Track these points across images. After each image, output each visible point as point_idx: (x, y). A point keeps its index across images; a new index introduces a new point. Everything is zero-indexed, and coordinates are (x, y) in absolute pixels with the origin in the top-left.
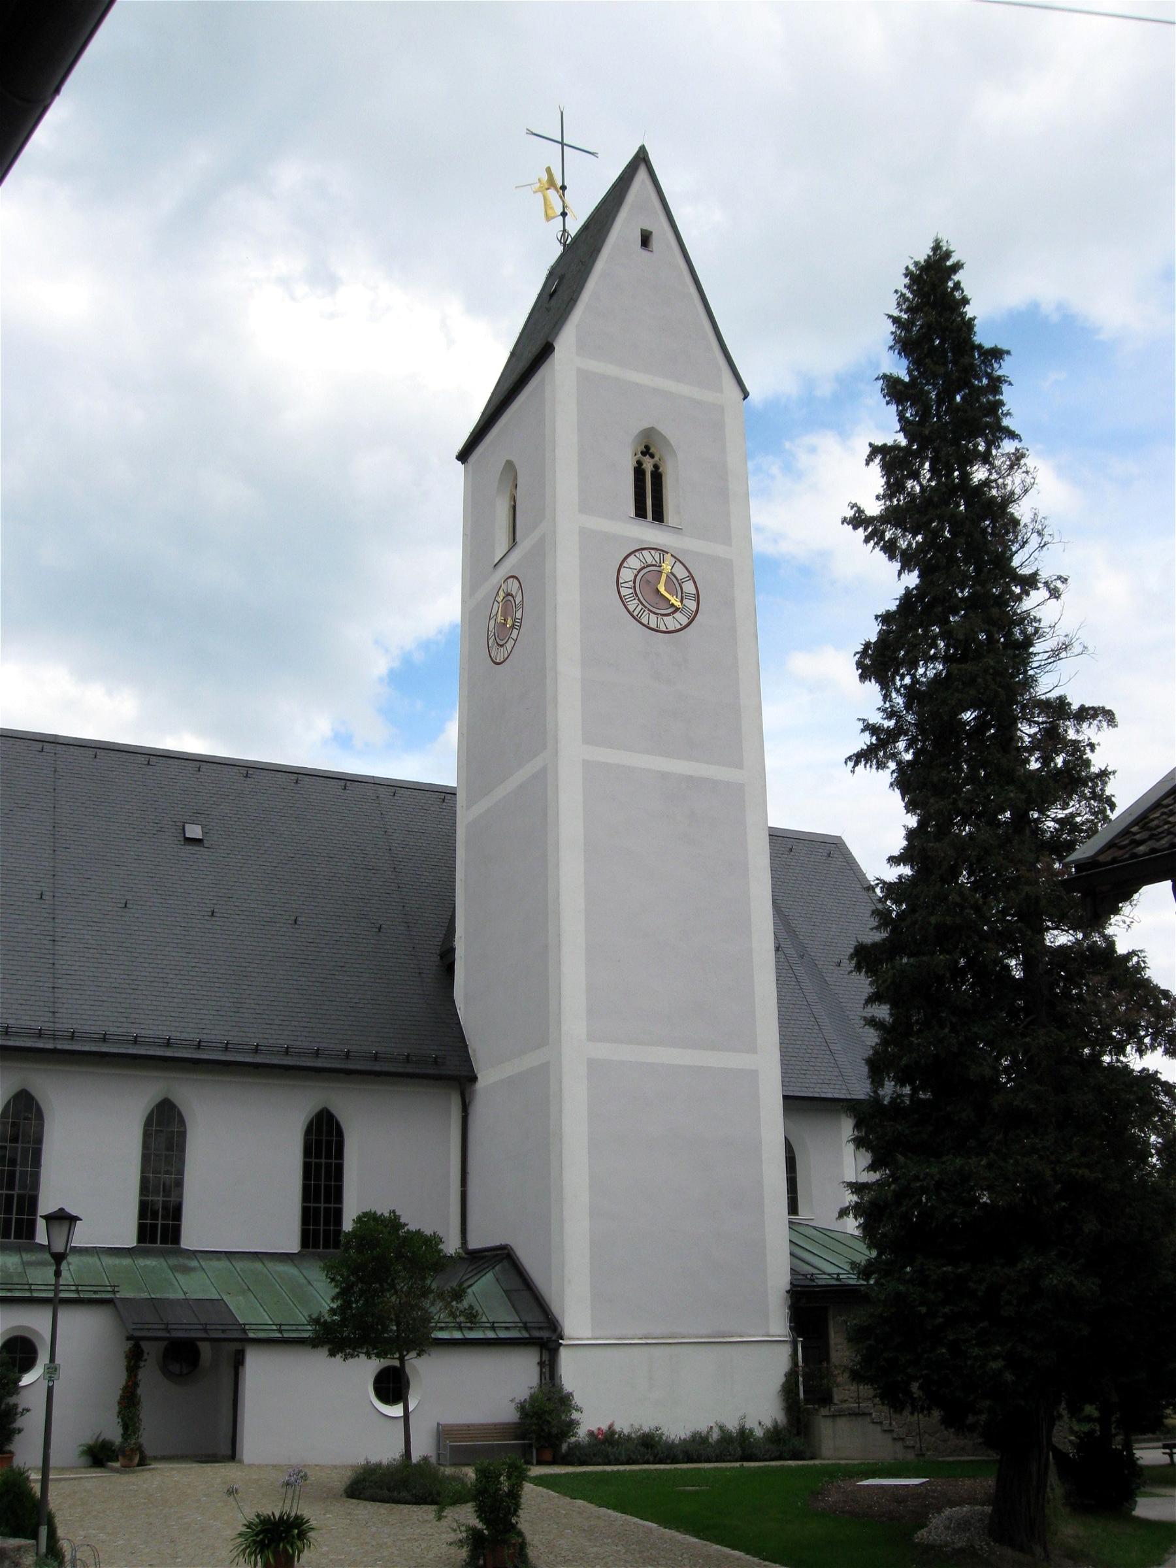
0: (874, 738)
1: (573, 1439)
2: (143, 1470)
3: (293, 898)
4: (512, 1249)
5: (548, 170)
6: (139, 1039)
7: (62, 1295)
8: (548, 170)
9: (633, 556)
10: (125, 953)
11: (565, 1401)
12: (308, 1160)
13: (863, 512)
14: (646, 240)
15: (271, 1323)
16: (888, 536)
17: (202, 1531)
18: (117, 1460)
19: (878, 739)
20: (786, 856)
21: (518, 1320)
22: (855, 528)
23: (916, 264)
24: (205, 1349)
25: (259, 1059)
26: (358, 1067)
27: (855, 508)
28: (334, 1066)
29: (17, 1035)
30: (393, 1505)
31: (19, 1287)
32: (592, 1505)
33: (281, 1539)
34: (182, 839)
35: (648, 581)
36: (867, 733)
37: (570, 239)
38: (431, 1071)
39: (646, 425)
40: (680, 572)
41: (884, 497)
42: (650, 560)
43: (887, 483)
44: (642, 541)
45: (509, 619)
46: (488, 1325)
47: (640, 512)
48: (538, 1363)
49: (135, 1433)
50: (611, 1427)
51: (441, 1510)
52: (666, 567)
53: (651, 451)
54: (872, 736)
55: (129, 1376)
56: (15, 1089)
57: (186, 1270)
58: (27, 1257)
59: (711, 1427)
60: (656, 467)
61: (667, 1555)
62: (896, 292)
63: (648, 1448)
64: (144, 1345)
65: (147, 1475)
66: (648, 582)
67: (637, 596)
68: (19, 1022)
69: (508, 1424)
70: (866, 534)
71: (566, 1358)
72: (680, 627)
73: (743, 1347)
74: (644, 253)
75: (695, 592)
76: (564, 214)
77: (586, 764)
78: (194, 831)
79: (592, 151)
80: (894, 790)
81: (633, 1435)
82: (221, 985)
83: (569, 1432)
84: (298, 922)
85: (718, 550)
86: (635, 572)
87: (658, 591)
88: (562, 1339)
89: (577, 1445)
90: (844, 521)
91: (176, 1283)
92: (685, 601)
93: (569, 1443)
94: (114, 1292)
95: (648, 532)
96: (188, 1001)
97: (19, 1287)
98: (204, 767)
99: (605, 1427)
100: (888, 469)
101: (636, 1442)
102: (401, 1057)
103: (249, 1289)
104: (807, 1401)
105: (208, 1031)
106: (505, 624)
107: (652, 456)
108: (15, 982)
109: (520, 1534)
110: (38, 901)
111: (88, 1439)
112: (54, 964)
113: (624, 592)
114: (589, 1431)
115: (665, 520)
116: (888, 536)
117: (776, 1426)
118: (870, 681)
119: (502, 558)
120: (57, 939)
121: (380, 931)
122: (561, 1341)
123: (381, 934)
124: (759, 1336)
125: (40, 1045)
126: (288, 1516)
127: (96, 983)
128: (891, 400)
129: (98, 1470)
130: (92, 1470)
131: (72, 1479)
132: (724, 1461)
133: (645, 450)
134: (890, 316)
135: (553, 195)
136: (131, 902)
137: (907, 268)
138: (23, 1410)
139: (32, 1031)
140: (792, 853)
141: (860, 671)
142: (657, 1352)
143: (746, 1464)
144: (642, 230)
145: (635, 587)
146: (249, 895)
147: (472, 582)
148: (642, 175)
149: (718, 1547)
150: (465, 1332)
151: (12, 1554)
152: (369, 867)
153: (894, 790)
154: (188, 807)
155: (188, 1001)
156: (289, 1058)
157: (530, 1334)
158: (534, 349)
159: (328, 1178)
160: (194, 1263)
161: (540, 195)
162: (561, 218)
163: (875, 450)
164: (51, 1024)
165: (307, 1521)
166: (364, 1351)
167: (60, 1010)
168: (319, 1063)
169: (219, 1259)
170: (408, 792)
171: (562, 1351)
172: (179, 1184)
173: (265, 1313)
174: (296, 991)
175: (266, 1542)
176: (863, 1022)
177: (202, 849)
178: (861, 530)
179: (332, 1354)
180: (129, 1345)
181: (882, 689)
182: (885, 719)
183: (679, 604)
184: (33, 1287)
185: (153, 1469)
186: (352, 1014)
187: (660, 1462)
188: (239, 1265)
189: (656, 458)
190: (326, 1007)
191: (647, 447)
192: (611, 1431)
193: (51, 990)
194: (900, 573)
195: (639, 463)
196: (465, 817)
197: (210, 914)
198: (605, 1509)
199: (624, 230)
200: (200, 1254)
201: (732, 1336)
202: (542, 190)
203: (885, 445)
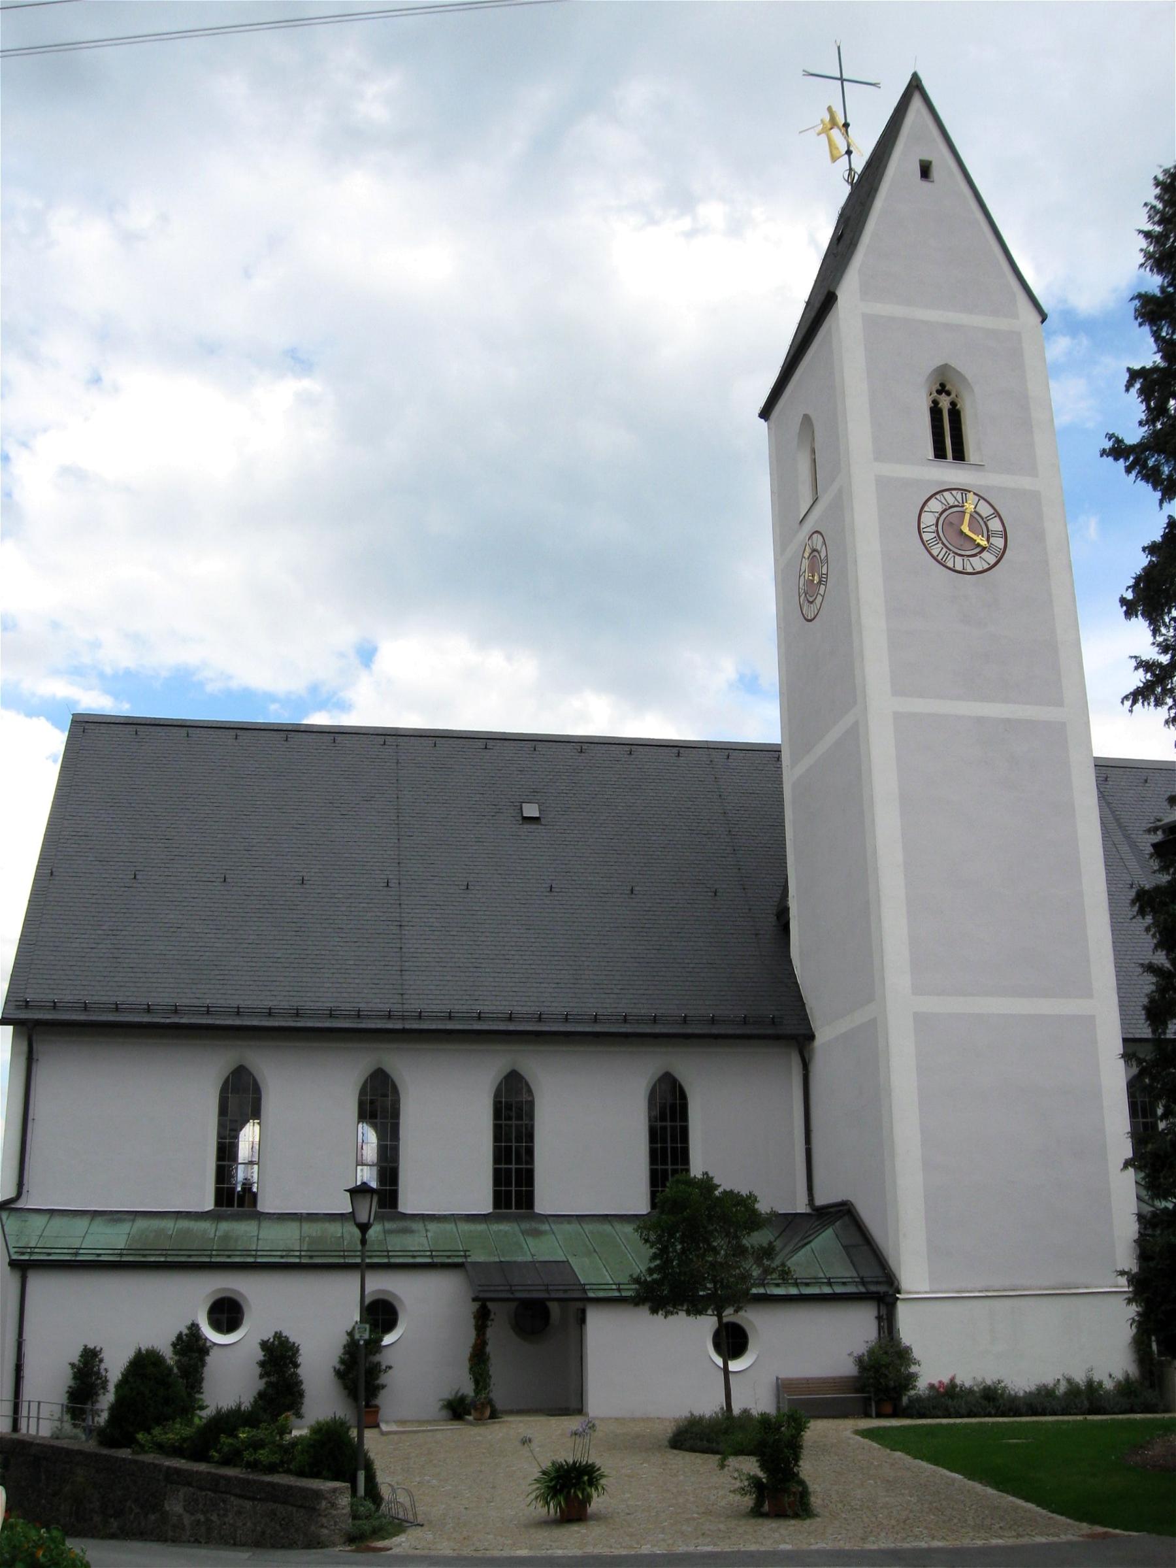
0: (1149, 674)
1: (912, 1392)
2: (495, 1423)
3: (629, 868)
4: (852, 1205)
5: (830, 109)
6: (482, 1015)
7: (368, 1261)
8: (830, 109)
9: (933, 499)
10: (594, 911)
11: (903, 1355)
12: (221, 1163)
13: (1122, 441)
14: (925, 171)
15: (611, 1282)
16: (1151, 463)
17: (524, 1478)
18: (470, 1414)
19: (1154, 675)
20: (1141, 788)
21: (855, 1275)
22: (1116, 459)
23: (1166, 171)
24: (554, 1308)
25: (598, 1028)
26: (697, 1031)
27: (1113, 439)
28: (671, 1031)
29: (369, 1017)
30: (710, 1455)
31: (378, 1253)
32: (909, 1457)
33: (574, 1485)
34: (520, 818)
35: (951, 523)
36: (1141, 670)
37: (856, 177)
38: (769, 1031)
39: (939, 362)
40: (985, 510)
41: (1147, 422)
42: (952, 501)
43: (1148, 407)
44: (944, 483)
45: (816, 574)
46: (825, 1281)
47: (940, 453)
48: (876, 1317)
49: (486, 1389)
50: (952, 1380)
51: (724, 1459)
52: (970, 507)
53: (947, 388)
54: (1146, 673)
55: (478, 1335)
56: (370, 1070)
57: (537, 1233)
58: (389, 1225)
59: (1059, 1380)
60: (953, 404)
61: (956, 1506)
62: (1146, 204)
63: (989, 1401)
64: (490, 1305)
65: (497, 1427)
66: (951, 523)
67: (940, 539)
68: (370, 1005)
69: (846, 1377)
70: (1127, 464)
71: (902, 1311)
72: (988, 566)
73: (1090, 1298)
74: (925, 185)
75: (1001, 529)
76: (849, 152)
77: (897, 716)
78: (531, 810)
79: (873, 82)
80: (1169, 727)
81: (975, 1388)
82: (560, 958)
83: (909, 1385)
84: (634, 892)
85: (1024, 482)
86: (937, 515)
87: (962, 533)
88: (899, 1293)
89: (919, 1399)
90: (1104, 453)
91: (526, 1247)
92: (992, 540)
93: (909, 1397)
94: (465, 1256)
95: (949, 473)
96: (530, 975)
97: (378, 1253)
98: (540, 746)
99: (946, 1380)
100: (1146, 394)
101: (978, 1395)
102: (738, 1019)
103: (595, 1251)
104: (1160, 1353)
105: (549, 1004)
106: (813, 581)
107: (948, 393)
108: (365, 967)
109: (802, 1483)
110: (385, 889)
111: (447, 1394)
112: (401, 948)
113: (926, 537)
114: (930, 1384)
115: (966, 458)
116: (1151, 463)
117: (1127, 1379)
118: (1137, 617)
119: (807, 512)
120: (403, 924)
121: (716, 895)
122: (898, 1295)
123: (717, 898)
124: (1107, 1287)
125: (390, 1026)
126: (580, 1464)
127: (440, 964)
128: (1144, 321)
129: (457, 1423)
130: (453, 1422)
131: (429, 1431)
132: (1070, 1414)
133: (940, 388)
134: (1140, 232)
135: (836, 134)
136: (473, 883)
137: (1155, 178)
138: (386, 1367)
139: (382, 1013)
140: (1147, 785)
141: (1125, 608)
142: (997, 1304)
143: (1090, 1417)
144: (921, 161)
145: (937, 531)
146: (586, 869)
147: (782, 542)
148: (917, 103)
149: (1011, 1498)
150: (767, 1288)
151: (328, 1495)
152: (703, 832)
153: (1169, 727)
154: (525, 787)
155: (530, 975)
156: (628, 1026)
157: (867, 1289)
158: (821, 298)
159: (674, 1140)
160: (545, 1227)
161: (823, 137)
162: (846, 156)
163: (1134, 375)
164: (400, 1006)
165: (599, 1469)
166: (685, 1308)
167: (408, 992)
168: (658, 1029)
169: (569, 1223)
170: (742, 754)
171: (900, 1305)
172: (530, 1152)
173: (607, 1274)
174: (633, 960)
175: (558, 1487)
176: (1140, 970)
177: (540, 827)
178: (1122, 460)
179: (654, 1311)
180: (475, 1306)
181: (1150, 624)
182: (1161, 653)
183: (986, 543)
184: (390, 1254)
185: (504, 1422)
186: (689, 979)
187: (1003, 1415)
188: (588, 1227)
189: (953, 395)
190: (663, 974)
191: (943, 385)
192: (952, 1384)
193: (399, 973)
194: (1161, 502)
195: (935, 402)
196: (791, 775)
197: (549, 889)
198: (920, 1461)
199: (901, 164)
200: (552, 1218)
201: (1078, 1288)
202: (826, 131)
203: (1143, 368)
